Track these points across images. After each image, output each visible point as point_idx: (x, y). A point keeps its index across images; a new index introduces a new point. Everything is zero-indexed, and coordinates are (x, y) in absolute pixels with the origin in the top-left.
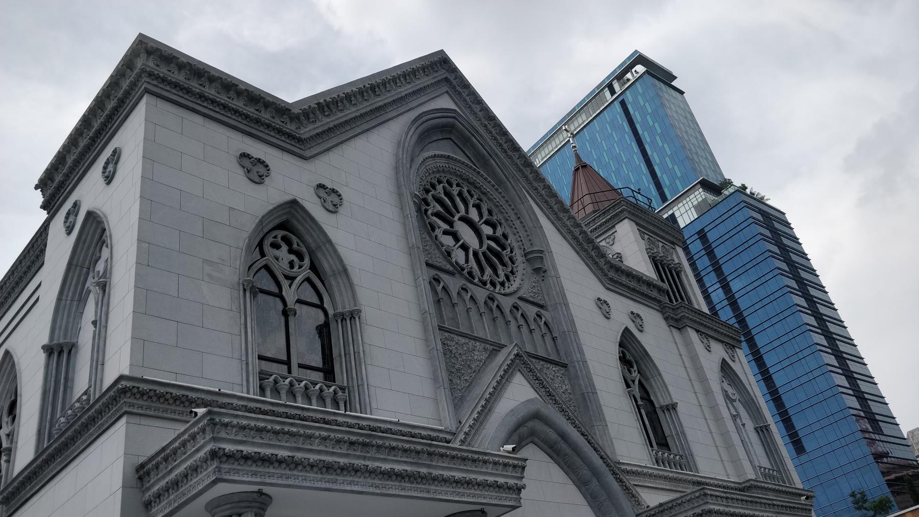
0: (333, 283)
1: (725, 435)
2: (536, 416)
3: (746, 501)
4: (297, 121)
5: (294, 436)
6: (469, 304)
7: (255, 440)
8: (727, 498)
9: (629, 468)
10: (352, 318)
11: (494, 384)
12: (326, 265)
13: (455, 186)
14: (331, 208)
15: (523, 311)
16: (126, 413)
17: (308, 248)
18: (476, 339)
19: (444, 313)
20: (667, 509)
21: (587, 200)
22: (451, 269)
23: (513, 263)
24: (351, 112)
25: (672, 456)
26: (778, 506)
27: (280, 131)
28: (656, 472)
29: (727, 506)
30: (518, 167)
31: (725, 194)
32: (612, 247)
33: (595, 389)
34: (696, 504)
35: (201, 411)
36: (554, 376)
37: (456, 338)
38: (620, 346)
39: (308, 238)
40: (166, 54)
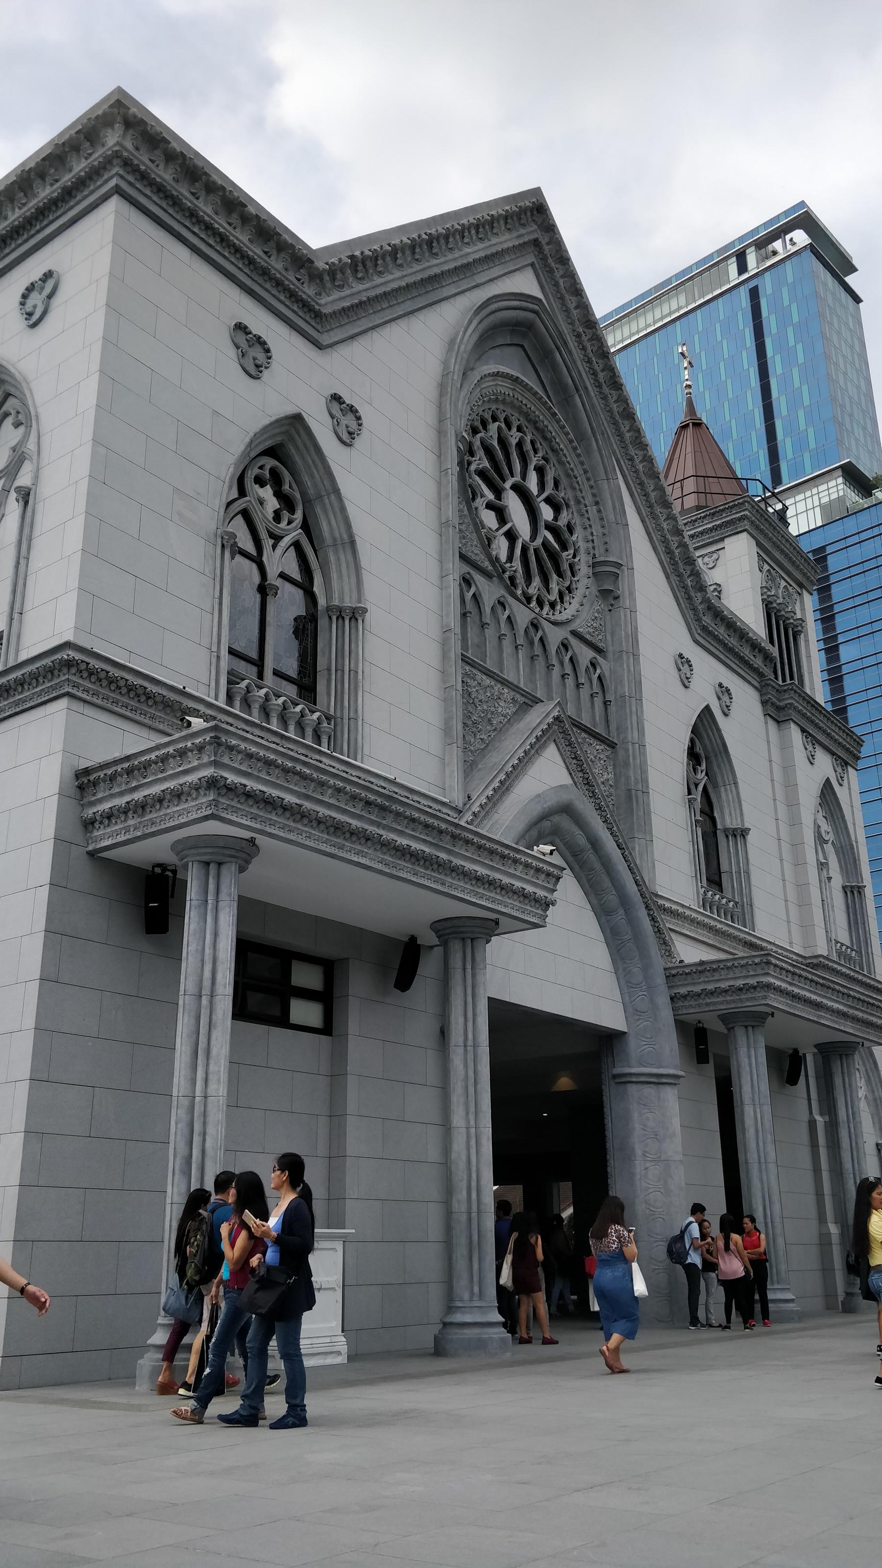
0: (332, 558)
1: (802, 887)
2: (567, 810)
3: (817, 983)
4: (318, 281)
5: (305, 779)
6: (504, 628)
7: (260, 775)
8: (794, 974)
9: (667, 905)
10: (354, 618)
11: (521, 753)
12: (326, 527)
13: (514, 430)
14: (345, 437)
16: (68, 694)
17: (303, 494)
18: (505, 683)
19: (469, 635)
20: (709, 971)
21: (690, 485)
22: (490, 568)
23: (573, 575)
24: (394, 278)
25: (724, 901)
26: (854, 997)
27: (292, 295)
28: (700, 918)
29: (790, 984)
30: (612, 417)
31: (877, 498)
32: (710, 571)
33: (648, 787)
34: (752, 973)
35: (197, 723)
36: (595, 757)
37: (479, 676)
38: (692, 732)
39: (306, 479)
40: (153, 131)
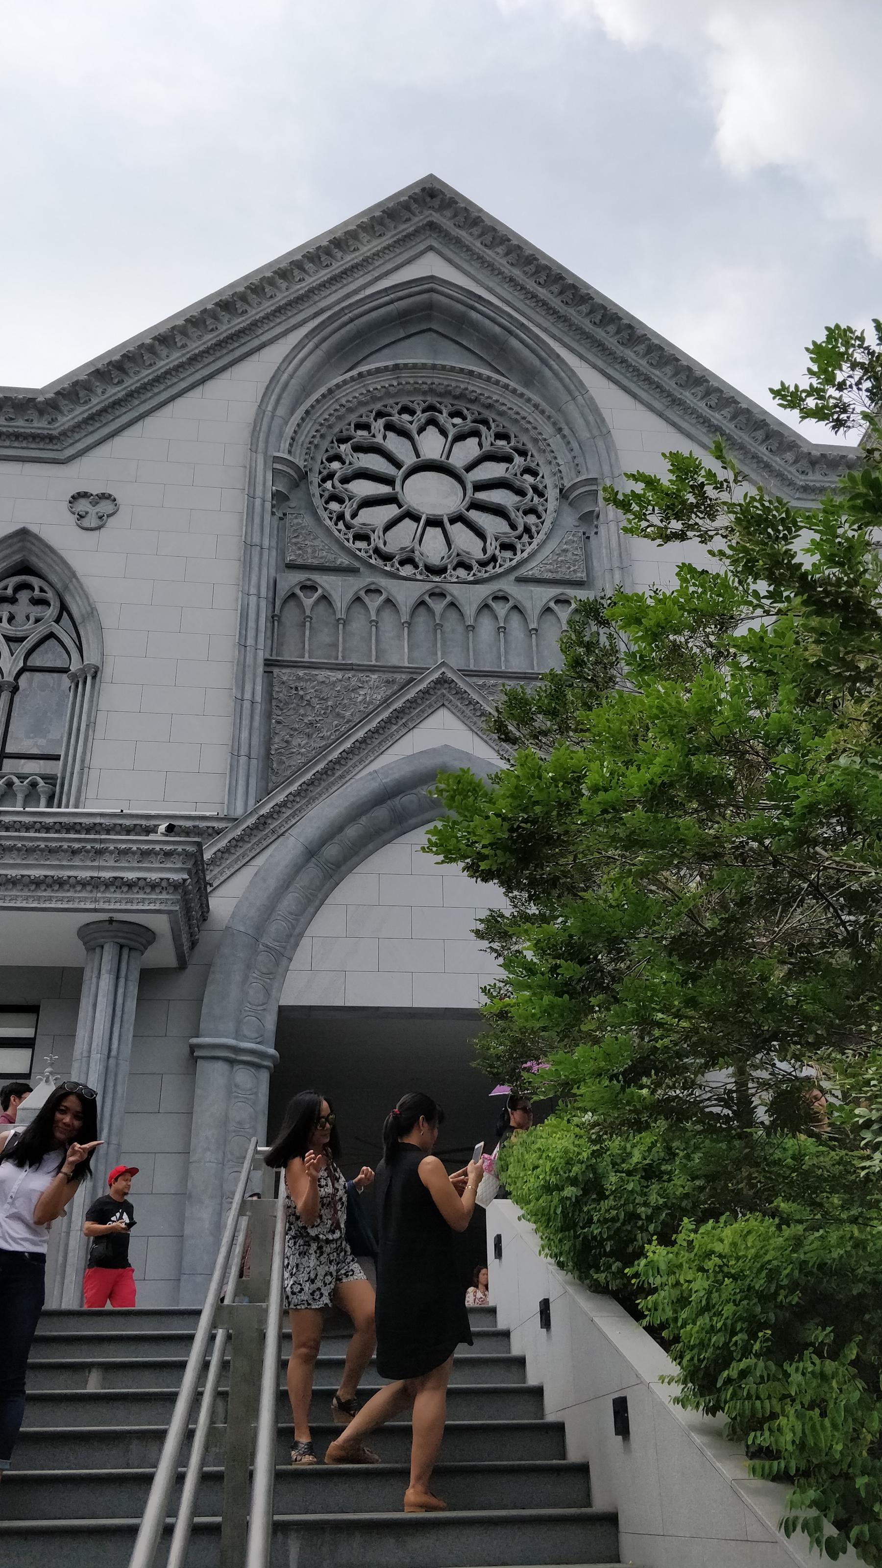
15: (550, 600)
39: (53, 578)
